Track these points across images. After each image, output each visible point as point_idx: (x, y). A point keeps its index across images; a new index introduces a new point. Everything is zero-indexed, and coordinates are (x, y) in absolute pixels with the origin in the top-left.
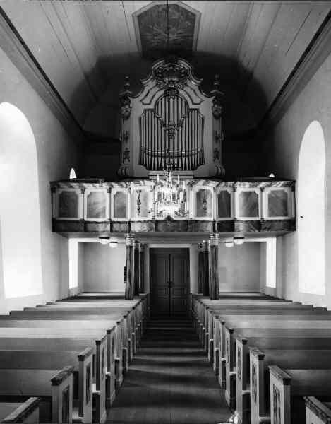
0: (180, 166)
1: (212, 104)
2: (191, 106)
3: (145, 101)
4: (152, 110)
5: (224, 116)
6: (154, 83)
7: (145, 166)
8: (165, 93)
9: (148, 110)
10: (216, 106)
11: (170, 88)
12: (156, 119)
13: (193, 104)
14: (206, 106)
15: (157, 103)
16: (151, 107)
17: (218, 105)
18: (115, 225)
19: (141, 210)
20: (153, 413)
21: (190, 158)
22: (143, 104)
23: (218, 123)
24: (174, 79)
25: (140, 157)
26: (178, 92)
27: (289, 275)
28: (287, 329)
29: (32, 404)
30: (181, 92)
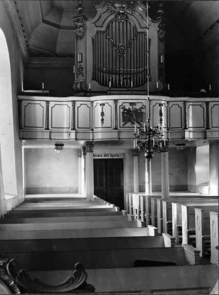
0: (99, 69)
1: (158, 29)
2: (139, 30)
3: (97, 24)
4: (103, 32)
5: (166, 40)
6: (105, 9)
7: (98, 81)
8: (116, 17)
9: (101, 32)
10: (161, 31)
11: (119, 14)
12: (107, 40)
13: (141, 28)
14: (152, 31)
15: (108, 27)
16: (103, 29)
17: (163, 30)
18: (52, 134)
19: (104, 121)
20: (214, 242)
21: (138, 75)
22: (96, 26)
23: (162, 44)
24: (124, 6)
25: (93, 74)
26: (127, 17)
27: (18, 121)
28: (46, 188)
29: (69, 279)
30: (130, 17)
